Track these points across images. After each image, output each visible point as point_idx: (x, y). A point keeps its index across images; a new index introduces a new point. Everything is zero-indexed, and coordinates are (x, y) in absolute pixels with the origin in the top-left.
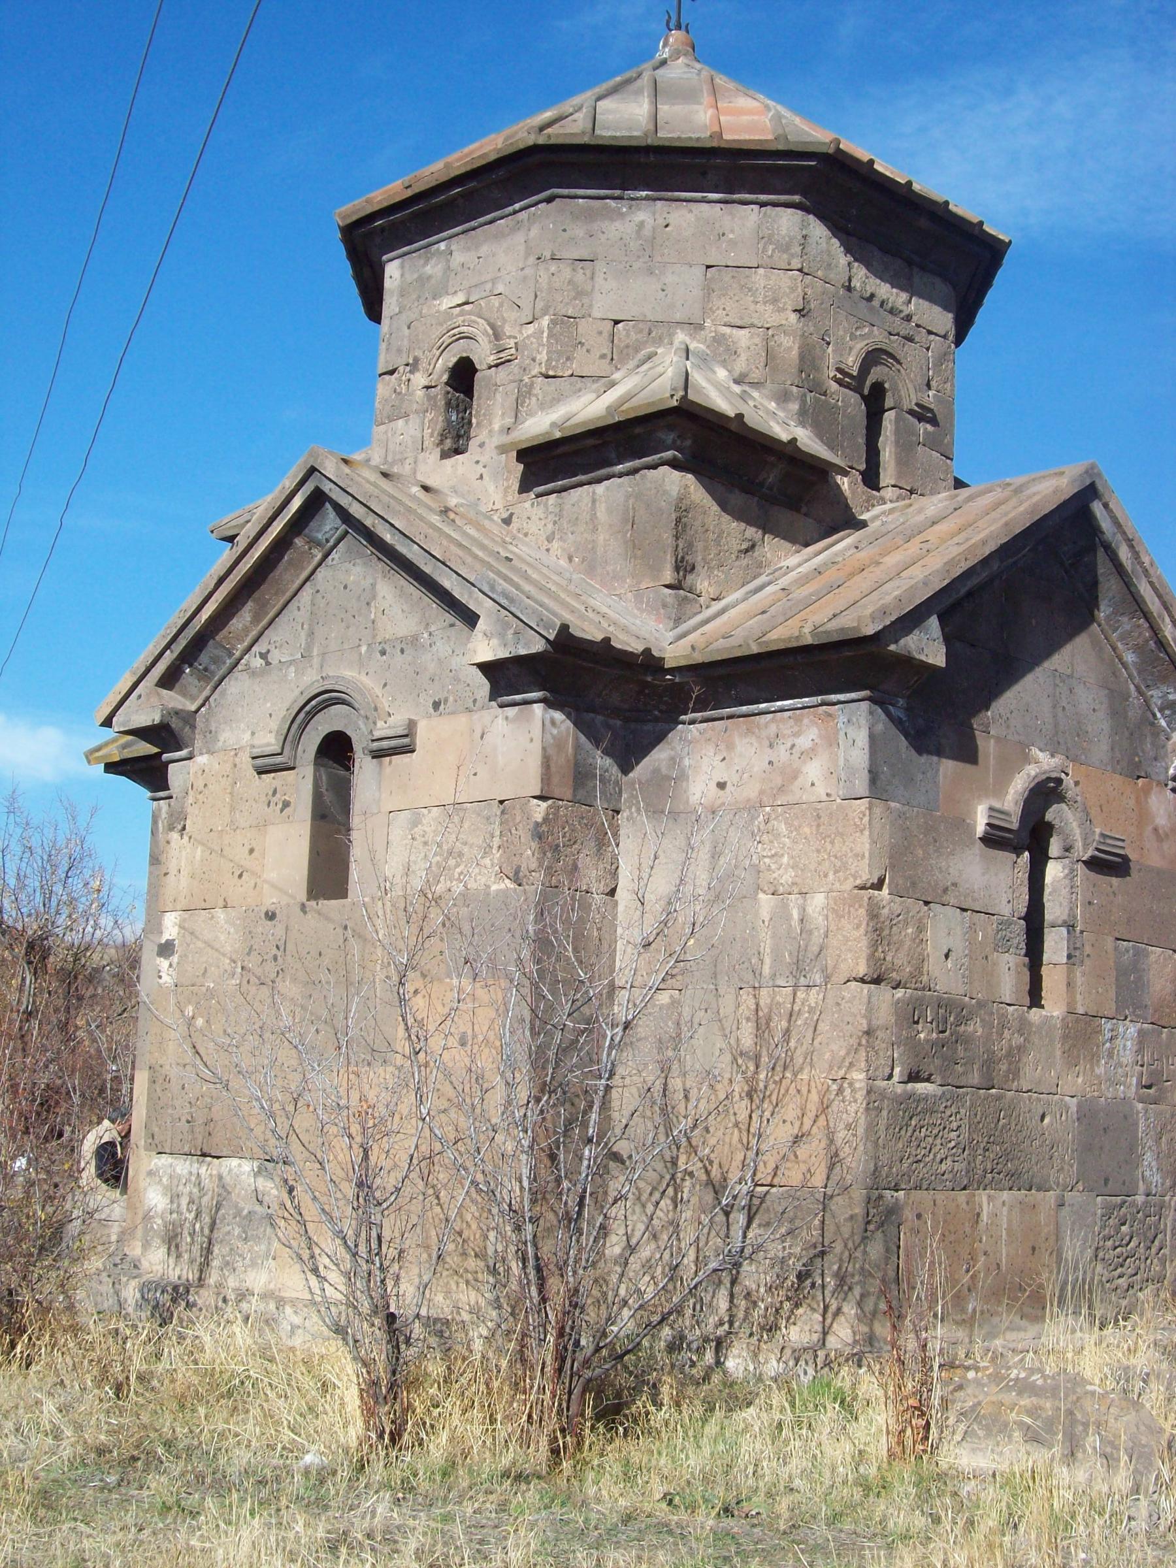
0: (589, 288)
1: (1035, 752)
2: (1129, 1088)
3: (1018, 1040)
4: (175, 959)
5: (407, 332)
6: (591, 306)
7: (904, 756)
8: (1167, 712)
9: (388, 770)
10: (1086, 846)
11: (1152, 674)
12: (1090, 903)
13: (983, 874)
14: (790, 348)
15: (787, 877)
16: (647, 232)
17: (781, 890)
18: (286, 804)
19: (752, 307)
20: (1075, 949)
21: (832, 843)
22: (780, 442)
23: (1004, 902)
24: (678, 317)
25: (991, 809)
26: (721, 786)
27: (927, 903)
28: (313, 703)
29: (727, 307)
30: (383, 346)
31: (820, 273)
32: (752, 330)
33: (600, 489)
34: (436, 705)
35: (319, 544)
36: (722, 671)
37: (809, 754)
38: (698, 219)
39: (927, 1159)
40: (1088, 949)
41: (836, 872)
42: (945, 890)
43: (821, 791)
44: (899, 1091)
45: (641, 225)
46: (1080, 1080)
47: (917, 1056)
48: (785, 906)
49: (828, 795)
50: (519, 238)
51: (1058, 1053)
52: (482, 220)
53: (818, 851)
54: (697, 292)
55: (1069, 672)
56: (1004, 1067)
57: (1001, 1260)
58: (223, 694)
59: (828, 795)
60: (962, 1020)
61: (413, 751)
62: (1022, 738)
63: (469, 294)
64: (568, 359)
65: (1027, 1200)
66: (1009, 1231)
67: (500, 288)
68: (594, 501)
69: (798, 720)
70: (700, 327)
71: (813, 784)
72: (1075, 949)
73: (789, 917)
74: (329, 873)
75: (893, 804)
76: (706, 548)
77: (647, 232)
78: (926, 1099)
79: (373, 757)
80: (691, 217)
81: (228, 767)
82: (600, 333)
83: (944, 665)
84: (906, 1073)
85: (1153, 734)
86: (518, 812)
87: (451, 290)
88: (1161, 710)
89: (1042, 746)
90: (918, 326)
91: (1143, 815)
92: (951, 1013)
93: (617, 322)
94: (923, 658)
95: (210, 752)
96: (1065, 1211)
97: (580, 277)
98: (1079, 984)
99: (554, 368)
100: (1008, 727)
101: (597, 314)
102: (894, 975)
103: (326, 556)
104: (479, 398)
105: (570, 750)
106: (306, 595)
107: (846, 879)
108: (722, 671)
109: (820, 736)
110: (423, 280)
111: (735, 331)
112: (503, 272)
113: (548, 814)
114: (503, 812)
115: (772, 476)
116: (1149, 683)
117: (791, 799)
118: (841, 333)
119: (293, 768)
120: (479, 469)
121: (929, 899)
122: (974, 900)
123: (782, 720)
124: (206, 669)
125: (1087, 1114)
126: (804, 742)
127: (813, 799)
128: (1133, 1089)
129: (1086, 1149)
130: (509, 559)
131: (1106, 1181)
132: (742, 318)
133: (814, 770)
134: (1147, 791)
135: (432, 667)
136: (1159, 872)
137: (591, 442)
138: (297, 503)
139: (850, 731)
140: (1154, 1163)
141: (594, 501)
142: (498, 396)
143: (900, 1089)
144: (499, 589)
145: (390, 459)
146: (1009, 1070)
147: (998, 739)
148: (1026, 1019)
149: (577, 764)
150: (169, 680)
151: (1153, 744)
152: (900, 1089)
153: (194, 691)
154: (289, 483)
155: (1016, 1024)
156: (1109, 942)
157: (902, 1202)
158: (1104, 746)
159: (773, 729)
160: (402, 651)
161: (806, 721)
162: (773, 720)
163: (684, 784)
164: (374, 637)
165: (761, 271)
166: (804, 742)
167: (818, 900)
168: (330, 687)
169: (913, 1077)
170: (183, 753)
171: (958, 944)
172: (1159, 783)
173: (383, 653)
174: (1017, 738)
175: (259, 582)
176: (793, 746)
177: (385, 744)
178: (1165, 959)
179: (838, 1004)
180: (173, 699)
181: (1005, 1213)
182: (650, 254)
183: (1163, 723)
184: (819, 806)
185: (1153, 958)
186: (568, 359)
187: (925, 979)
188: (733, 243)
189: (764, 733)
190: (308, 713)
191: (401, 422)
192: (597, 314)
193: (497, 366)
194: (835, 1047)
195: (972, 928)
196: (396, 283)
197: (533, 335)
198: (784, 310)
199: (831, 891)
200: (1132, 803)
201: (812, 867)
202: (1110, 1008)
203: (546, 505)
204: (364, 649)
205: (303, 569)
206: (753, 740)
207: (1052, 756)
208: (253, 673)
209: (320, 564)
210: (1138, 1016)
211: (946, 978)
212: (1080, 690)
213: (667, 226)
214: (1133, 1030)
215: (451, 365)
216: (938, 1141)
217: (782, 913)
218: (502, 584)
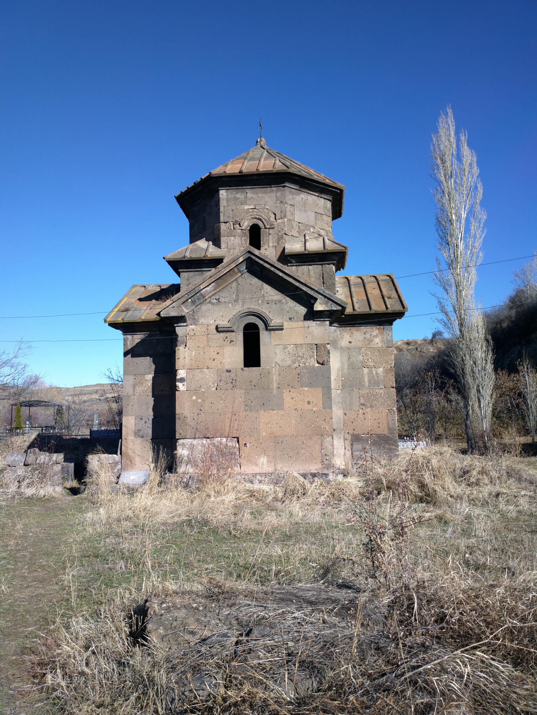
5: (231, 212)
26: (350, 342)
33: (310, 267)
35: (240, 272)
37: (376, 336)
67: (267, 207)
73: (373, 373)
81: (205, 330)
83: (315, 309)
104: (263, 236)
106: (234, 284)
110: (236, 199)
112: (268, 203)
117: (371, 346)
133: (377, 340)
139: (387, 332)
145: (229, 247)
170: (185, 324)
173: (268, 303)
191: (232, 238)
197: (282, 222)
217: (371, 372)
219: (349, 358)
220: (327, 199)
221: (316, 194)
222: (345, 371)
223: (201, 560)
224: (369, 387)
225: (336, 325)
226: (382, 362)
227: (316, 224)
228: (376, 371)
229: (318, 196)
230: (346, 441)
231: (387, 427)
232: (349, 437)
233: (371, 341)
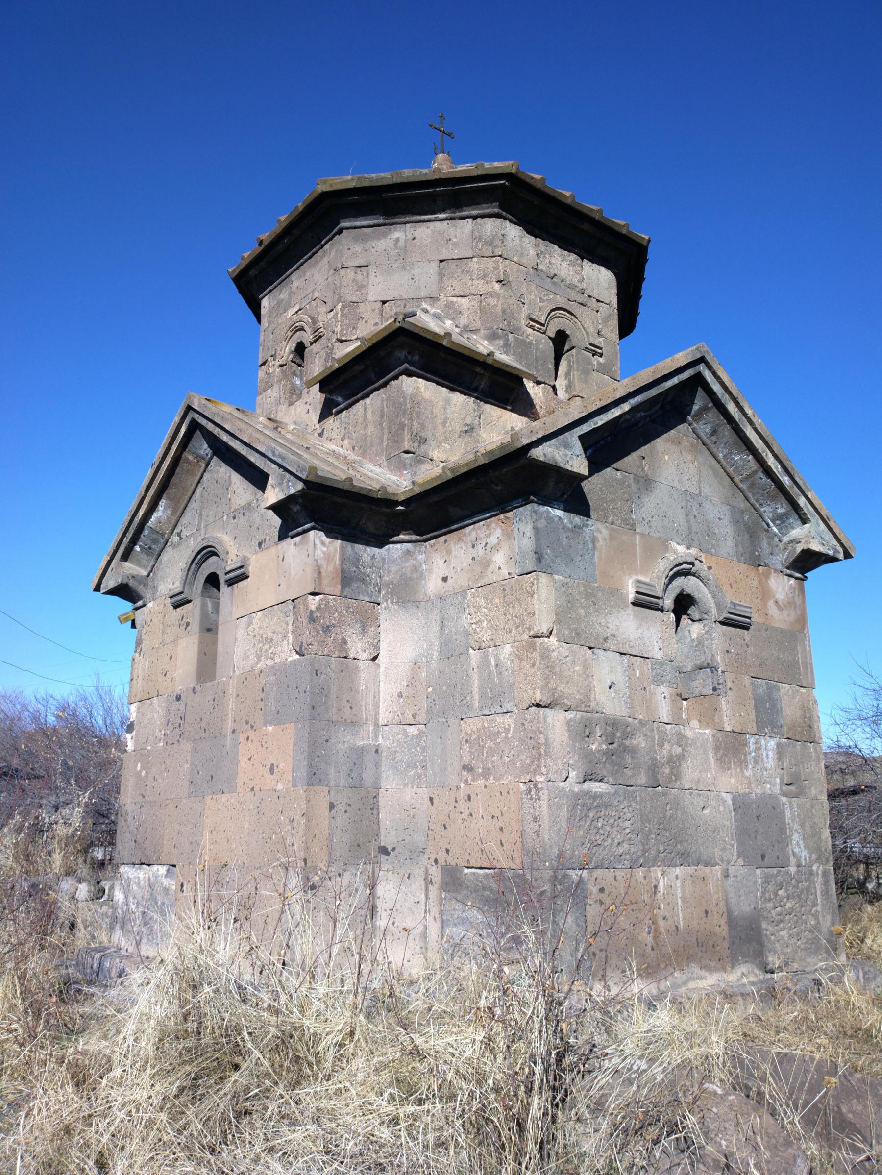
0: (365, 283)
1: (674, 545)
2: (774, 787)
3: (678, 750)
4: (134, 733)
6: (367, 294)
7: (564, 543)
8: (778, 522)
9: (236, 591)
10: (719, 611)
11: (763, 495)
12: (728, 651)
13: (637, 629)
14: (496, 305)
15: (486, 636)
16: (401, 244)
17: (483, 645)
18: (188, 624)
19: (470, 283)
20: (719, 684)
21: (514, 607)
22: (480, 354)
23: (657, 649)
24: (423, 295)
25: (638, 581)
26: (445, 579)
27: (590, 648)
28: (199, 557)
29: (454, 285)
30: (261, 348)
31: (515, 259)
32: (471, 297)
33: (368, 401)
34: (260, 544)
36: (435, 498)
37: (496, 548)
38: (433, 232)
39: (606, 844)
40: (729, 684)
41: (517, 627)
42: (606, 639)
43: (504, 572)
44: (576, 790)
45: (398, 239)
46: (733, 780)
47: (590, 763)
48: (486, 658)
49: (509, 574)
50: (325, 261)
51: (712, 761)
52: (306, 257)
53: (505, 614)
54: (435, 278)
55: (697, 492)
56: (667, 771)
57: (679, 923)
58: (160, 563)
59: (509, 574)
60: (627, 735)
61: (247, 577)
62: (662, 535)
63: (301, 304)
64: (354, 328)
65: (697, 873)
66: (684, 899)
67: (316, 295)
68: (365, 409)
69: (489, 526)
70: (437, 299)
71: (500, 568)
72: (719, 684)
74: (207, 665)
75: (556, 577)
76: (434, 428)
77: (401, 244)
78: (601, 796)
79: (229, 586)
80: (428, 231)
82: (373, 310)
84: (582, 776)
85: (768, 537)
86: (301, 606)
87: (292, 304)
88: (773, 521)
89: (680, 541)
90: (590, 297)
91: (765, 594)
92: (617, 731)
93: (384, 302)
94: (570, 468)
95: (154, 599)
96: (731, 881)
97: (359, 277)
98: (725, 709)
99: (346, 335)
100: (650, 527)
101: (371, 298)
102: (566, 701)
103: (207, 465)
105: (338, 562)
107: (524, 631)
108: (435, 498)
109: (503, 534)
111: (459, 299)
113: (320, 605)
114: (294, 607)
115: (483, 383)
116: (761, 502)
117: (487, 581)
118: (533, 297)
119: (190, 601)
120: (307, 407)
121: (592, 646)
122: (631, 647)
123: (479, 528)
124: (150, 548)
125: (741, 804)
126: (493, 540)
127: (501, 578)
128: (778, 787)
129: (743, 833)
130: (308, 448)
131: (763, 857)
132: (463, 291)
133: (499, 558)
134: (767, 576)
135: (258, 520)
136: (782, 631)
137: (359, 367)
138: (183, 430)
140: (801, 842)
141: (365, 409)
142: (316, 359)
143: (577, 788)
144: (277, 453)
146: (672, 773)
147: (642, 535)
148: (683, 735)
149: (343, 571)
150: (125, 557)
151: (769, 544)
152: (577, 788)
153: (146, 563)
154: (177, 419)
155: (675, 739)
156: (747, 680)
157: (586, 879)
158: (730, 544)
159: (474, 534)
160: (244, 514)
161: (493, 525)
162: (473, 529)
163: (423, 582)
164: (230, 509)
165: (475, 260)
166: (493, 540)
167: (508, 649)
168: (205, 545)
169: (588, 777)
171: (620, 678)
172: (776, 570)
173: (234, 518)
174: (658, 535)
175: (167, 482)
176: (486, 544)
177: (232, 575)
178: (793, 692)
179: (523, 724)
180: (130, 568)
181: (679, 885)
182: (403, 258)
183: (775, 529)
184: (504, 582)
185: (782, 691)
186: (354, 328)
187: (593, 704)
188: (456, 244)
189: (468, 539)
190: (197, 564)
192: (371, 298)
193: (315, 342)
194: (523, 757)
195: (631, 666)
196: (267, 309)
198: (491, 281)
199: (515, 642)
200: (755, 583)
201: (502, 627)
202: (752, 727)
203: (340, 419)
204: (225, 518)
205: (196, 475)
206: (462, 545)
207: (688, 548)
208: (174, 546)
209: (205, 471)
210: (776, 733)
211: (612, 705)
212: (707, 505)
213: (414, 239)
214: (772, 743)
215: (293, 349)
216: (615, 829)
217: (484, 662)
218: (279, 450)
219: (442, 626)
220: (483, 216)
221: (442, 216)
222: (434, 665)
223: (595, 1049)
224: (481, 708)
225: (407, 537)
226: (509, 626)
227: (441, 289)
228: (497, 657)
229: (451, 219)
230: (430, 886)
231: (519, 844)
232: (436, 873)
233: (486, 564)
